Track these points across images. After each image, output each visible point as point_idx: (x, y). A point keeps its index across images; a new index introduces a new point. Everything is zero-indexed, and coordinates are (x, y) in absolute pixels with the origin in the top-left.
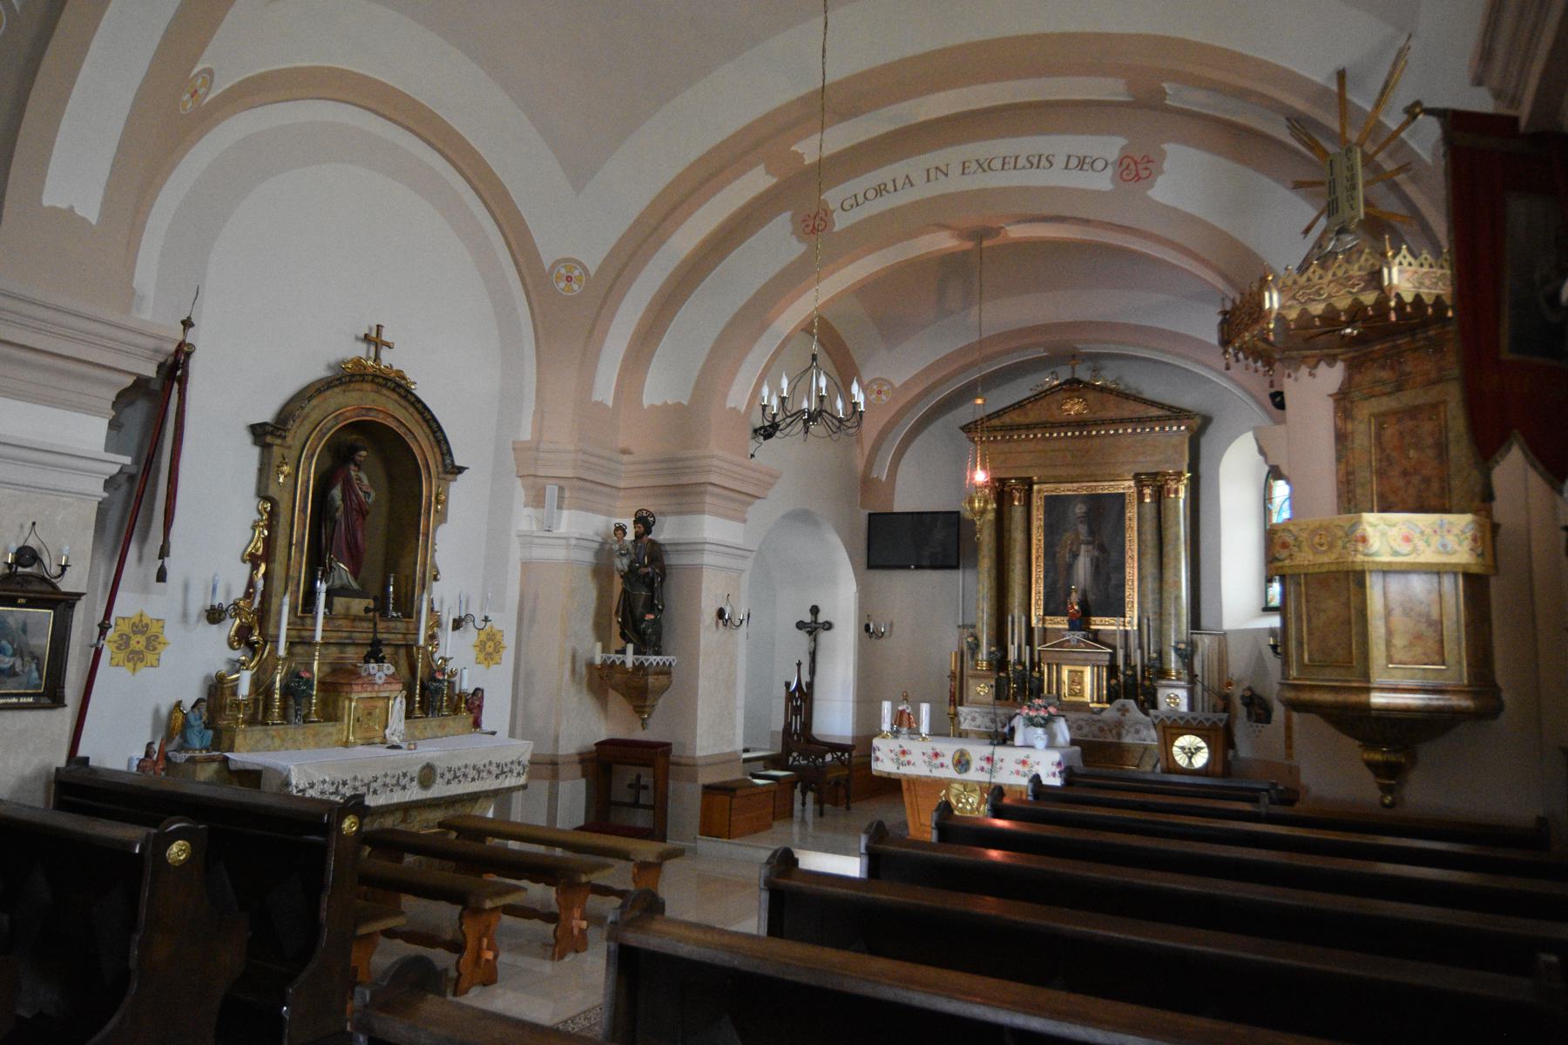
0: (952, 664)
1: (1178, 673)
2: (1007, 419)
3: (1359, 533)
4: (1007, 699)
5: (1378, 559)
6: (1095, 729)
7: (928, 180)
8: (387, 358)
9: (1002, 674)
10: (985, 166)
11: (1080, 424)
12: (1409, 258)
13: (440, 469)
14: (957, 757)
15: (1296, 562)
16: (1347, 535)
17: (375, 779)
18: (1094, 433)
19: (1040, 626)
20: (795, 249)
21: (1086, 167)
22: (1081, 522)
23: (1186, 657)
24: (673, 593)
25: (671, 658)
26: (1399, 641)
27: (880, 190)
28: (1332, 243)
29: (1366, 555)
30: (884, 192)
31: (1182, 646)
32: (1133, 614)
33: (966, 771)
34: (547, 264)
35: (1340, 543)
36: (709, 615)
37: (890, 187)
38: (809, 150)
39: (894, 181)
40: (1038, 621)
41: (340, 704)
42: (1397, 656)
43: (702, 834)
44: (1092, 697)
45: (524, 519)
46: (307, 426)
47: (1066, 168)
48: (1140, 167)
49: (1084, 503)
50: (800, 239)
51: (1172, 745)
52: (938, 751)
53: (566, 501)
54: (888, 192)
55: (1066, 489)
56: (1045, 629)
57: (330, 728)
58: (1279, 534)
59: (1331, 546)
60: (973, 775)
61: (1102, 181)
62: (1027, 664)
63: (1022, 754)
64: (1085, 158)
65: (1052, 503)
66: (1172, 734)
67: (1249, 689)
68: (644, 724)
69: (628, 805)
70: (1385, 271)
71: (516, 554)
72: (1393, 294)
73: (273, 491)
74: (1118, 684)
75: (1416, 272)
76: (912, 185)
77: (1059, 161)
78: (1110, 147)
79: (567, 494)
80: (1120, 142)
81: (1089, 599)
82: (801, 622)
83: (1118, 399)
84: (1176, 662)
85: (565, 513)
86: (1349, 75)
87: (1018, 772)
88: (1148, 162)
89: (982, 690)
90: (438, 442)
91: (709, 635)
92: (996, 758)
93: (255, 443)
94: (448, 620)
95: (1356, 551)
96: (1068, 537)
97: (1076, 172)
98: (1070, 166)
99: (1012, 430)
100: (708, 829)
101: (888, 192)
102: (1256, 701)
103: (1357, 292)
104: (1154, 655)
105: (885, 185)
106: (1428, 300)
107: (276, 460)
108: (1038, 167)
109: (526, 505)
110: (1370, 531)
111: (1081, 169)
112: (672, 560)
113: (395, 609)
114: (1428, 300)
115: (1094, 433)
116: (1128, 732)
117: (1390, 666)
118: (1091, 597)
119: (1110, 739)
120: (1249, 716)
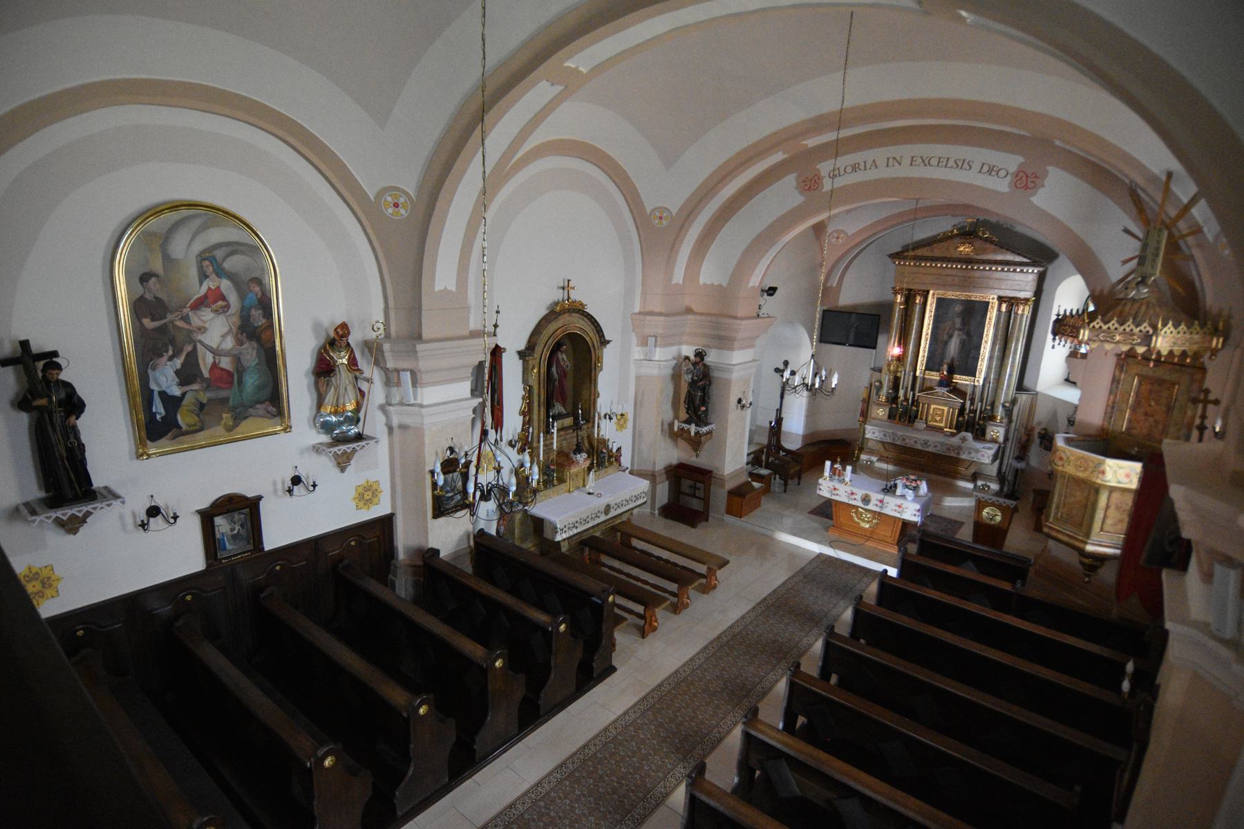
0: (864, 394)
1: (1002, 418)
2: (919, 252)
3: (1101, 469)
4: (895, 419)
5: (1108, 484)
6: (944, 448)
7: (888, 166)
8: (574, 296)
9: (894, 406)
10: (926, 162)
11: (968, 261)
12: (1172, 329)
13: (599, 344)
14: (863, 497)
15: (1065, 470)
16: (1095, 467)
17: (588, 517)
18: (975, 268)
19: (922, 375)
20: (799, 199)
21: (993, 173)
22: (958, 316)
23: (1009, 410)
24: (714, 391)
25: (712, 426)
26: (1109, 521)
27: (855, 168)
28: (1134, 293)
29: (1102, 480)
30: (857, 169)
31: (1007, 405)
32: (980, 379)
33: (867, 505)
34: (648, 210)
35: (1090, 469)
36: (733, 400)
37: (862, 166)
38: (811, 142)
39: (865, 162)
40: (921, 373)
41: (565, 473)
42: (1106, 528)
43: (727, 513)
44: (946, 423)
45: (637, 353)
46: (542, 345)
47: (980, 172)
48: (1029, 180)
49: (962, 305)
50: (801, 193)
51: (982, 511)
52: (854, 492)
53: (658, 343)
54: (860, 170)
55: (951, 295)
56: (924, 378)
57: (563, 486)
58: (1060, 452)
59: (1086, 469)
60: (871, 507)
61: (1002, 185)
62: (910, 401)
63: (899, 501)
64: (994, 167)
65: (941, 302)
66: (983, 505)
67: (1045, 429)
68: (697, 456)
69: (689, 495)
70: (1154, 338)
71: (633, 372)
72: (1155, 352)
73: (531, 383)
74: (963, 420)
75: (1174, 337)
76: (876, 167)
77: (976, 167)
78: (1012, 162)
79: (659, 339)
80: (1021, 159)
81: (955, 363)
82: (778, 368)
83: (996, 247)
84: (1002, 412)
85: (658, 349)
86: (1174, 176)
87: (896, 510)
88: (1036, 177)
89: (881, 412)
90: (598, 332)
91: (733, 413)
92: (885, 501)
93: (520, 359)
94: (602, 415)
95: (1098, 477)
96: (948, 325)
97: (987, 175)
98: (983, 171)
99: (921, 259)
100: (729, 511)
101: (860, 170)
102: (1047, 438)
103: (1136, 344)
104: (989, 408)
105: (859, 164)
106: (1177, 353)
107: (531, 367)
108: (961, 168)
109: (637, 346)
110: (1108, 469)
111: (990, 174)
112: (715, 374)
113: (582, 420)
114: (1177, 353)
115: (975, 268)
116: (964, 453)
117: (1102, 533)
118: (956, 363)
119: (953, 454)
120: (1041, 443)
